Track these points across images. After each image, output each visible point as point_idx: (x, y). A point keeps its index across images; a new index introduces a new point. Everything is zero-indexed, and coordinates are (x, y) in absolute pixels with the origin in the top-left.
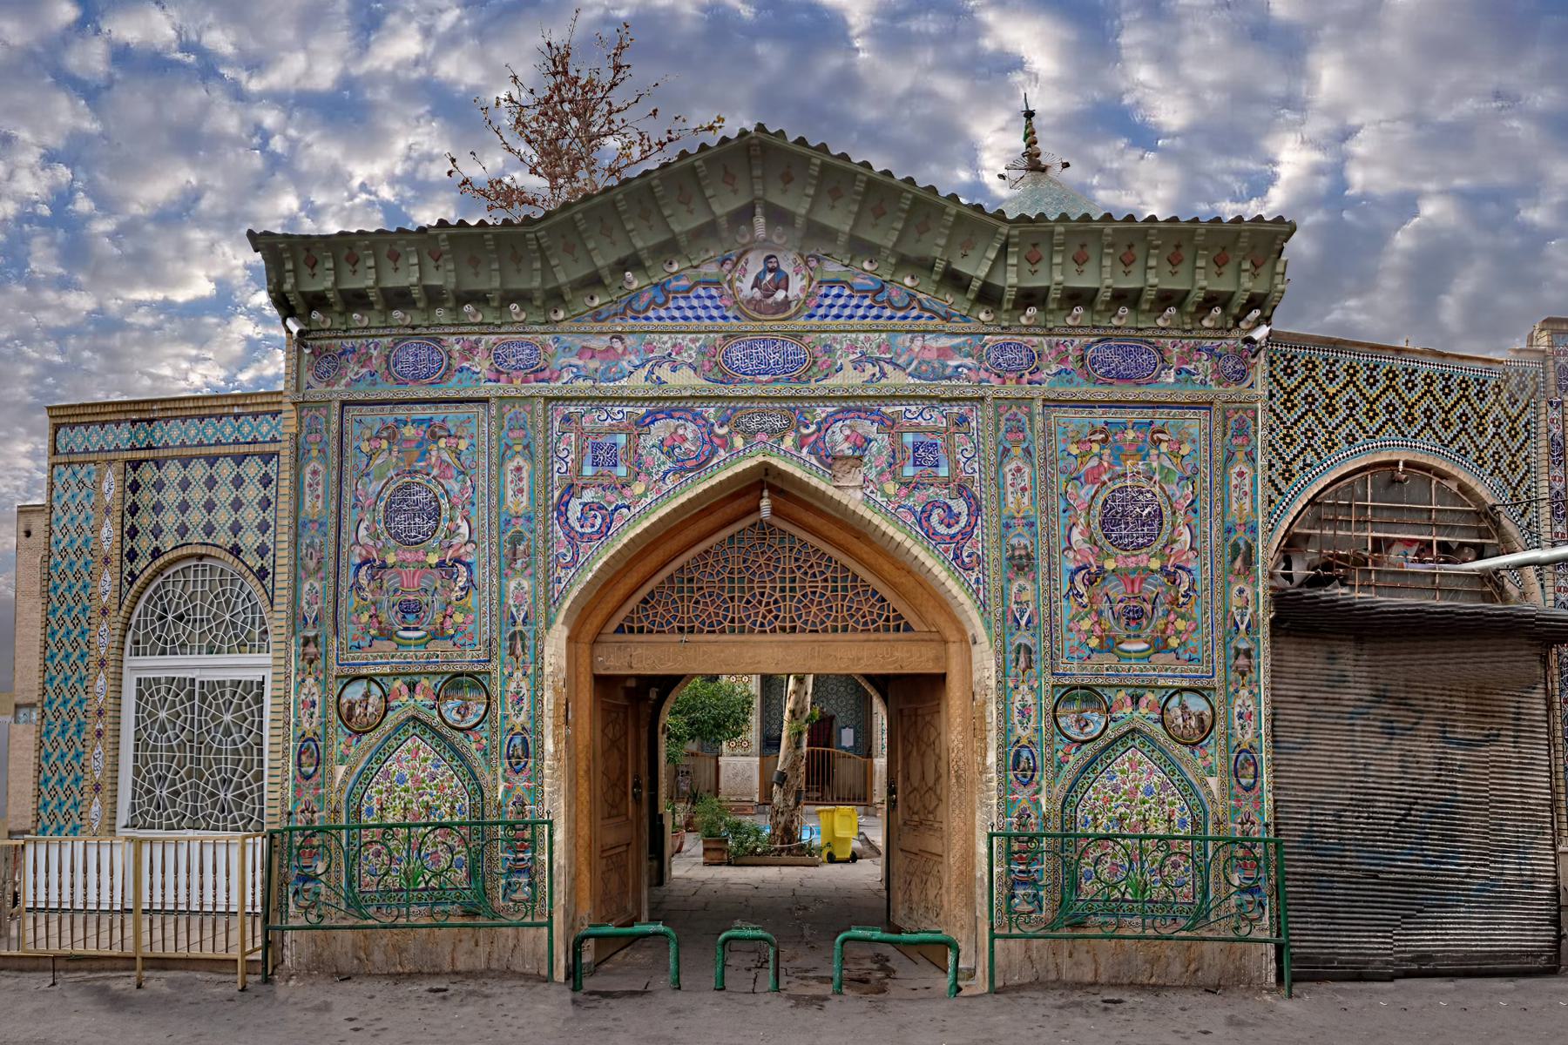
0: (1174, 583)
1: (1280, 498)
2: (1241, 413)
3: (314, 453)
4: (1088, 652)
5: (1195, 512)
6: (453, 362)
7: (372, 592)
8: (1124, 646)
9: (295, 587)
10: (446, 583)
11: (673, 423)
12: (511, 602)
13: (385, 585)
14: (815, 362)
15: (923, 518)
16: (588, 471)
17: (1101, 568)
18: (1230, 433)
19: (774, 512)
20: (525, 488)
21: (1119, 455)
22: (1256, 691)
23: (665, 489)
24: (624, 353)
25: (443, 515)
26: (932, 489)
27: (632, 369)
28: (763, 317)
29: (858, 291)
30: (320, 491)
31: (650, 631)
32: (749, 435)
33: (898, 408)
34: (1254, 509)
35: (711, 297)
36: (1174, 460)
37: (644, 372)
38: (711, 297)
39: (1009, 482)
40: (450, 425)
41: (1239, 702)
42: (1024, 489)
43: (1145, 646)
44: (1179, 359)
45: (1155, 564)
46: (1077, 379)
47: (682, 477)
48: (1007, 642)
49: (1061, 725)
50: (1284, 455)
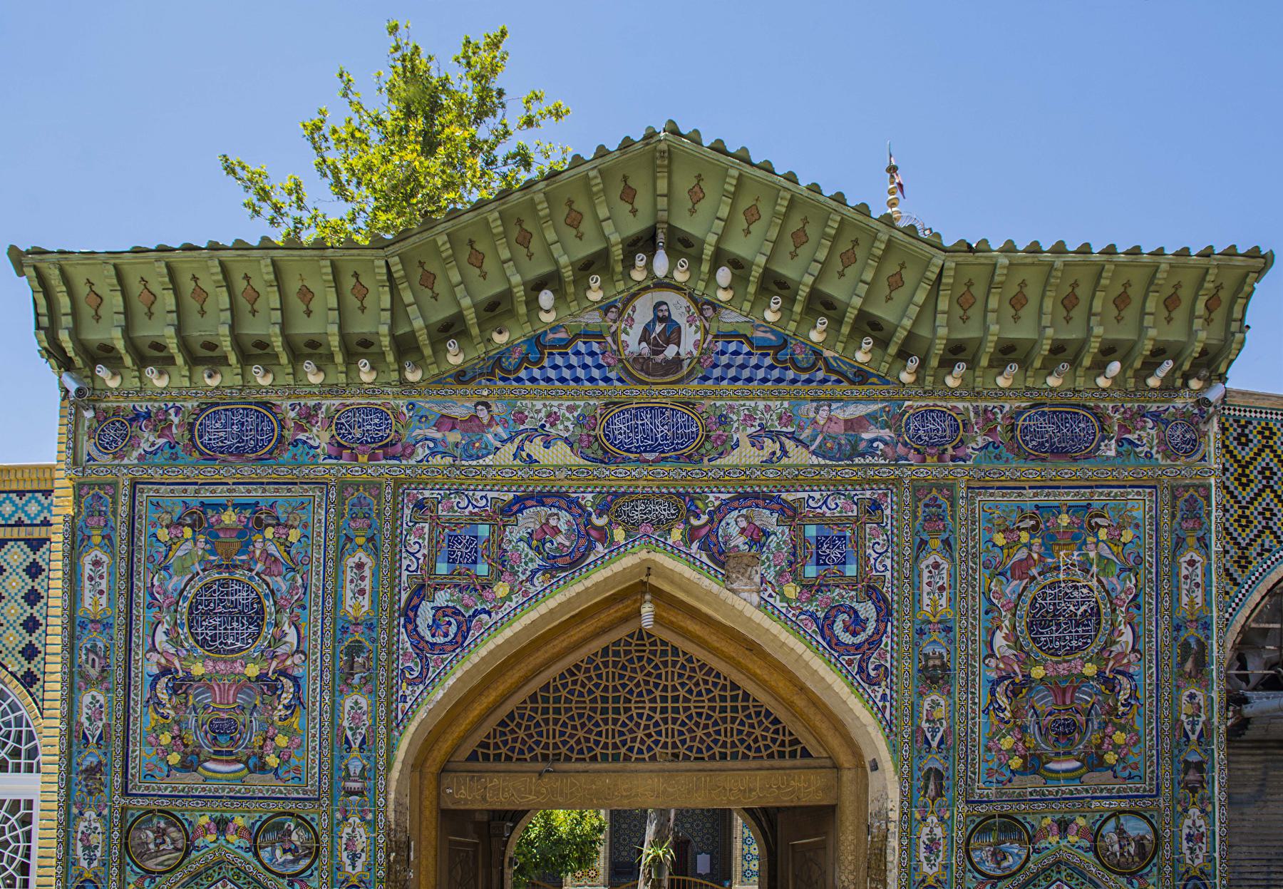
0: (1112, 690)
1: (1236, 588)
2: (1191, 490)
3: (97, 540)
4: (1009, 774)
5: (1138, 607)
6: (286, 433)
7: (174, 708)
8: (1051, 766)
9: (71, 699)
10: (268, 699)
11: (544, 511)
12: (346, 724)
13: (191, 700)
14: (708, 437)
15: (825, 627)
16: (442, 568)
17: (1027, 677)
18: (1179, 515)
19: (658, 620)
20: (367, 588)
21: (1052, 540)
22: (1209, 808)
23: (532, 591)
24: (490, 425)
25: (267, 620)
26: (837, 591)
27: (498, 444)
28: (650, 379)
29: (758, 348)
30: (104, 585)
31: (509, 758)
32: (631, 528)
33: (800, 495)
34: (1207, 603)
35: (592, 354)
36: (1115, 549)
37: (511, 448)
38: (592, 354)
39: (926, 580)
40: (280, 512)
41: (1188, 822)
42: (942, 588)
43: (1078, 764)
44: (1120, 426)
45: (1090, 670)
46: (1005, 454)
47: (553, 577)
48: (915, 768)
49: (975, 860)
50: (1239, 540)
